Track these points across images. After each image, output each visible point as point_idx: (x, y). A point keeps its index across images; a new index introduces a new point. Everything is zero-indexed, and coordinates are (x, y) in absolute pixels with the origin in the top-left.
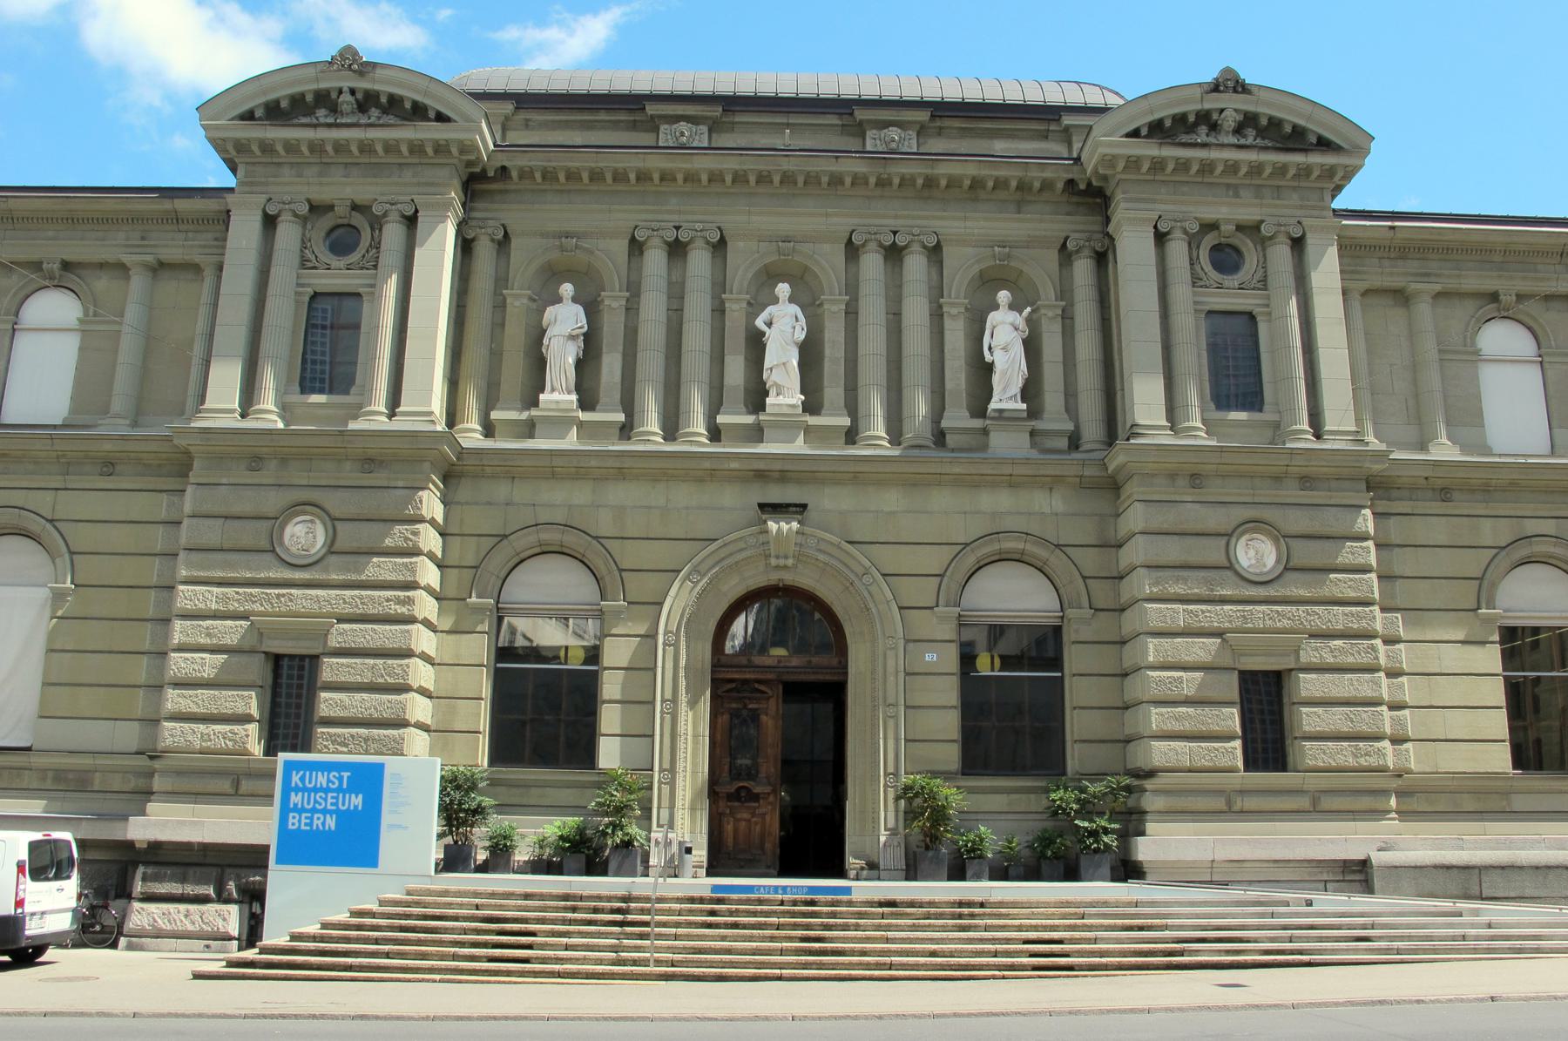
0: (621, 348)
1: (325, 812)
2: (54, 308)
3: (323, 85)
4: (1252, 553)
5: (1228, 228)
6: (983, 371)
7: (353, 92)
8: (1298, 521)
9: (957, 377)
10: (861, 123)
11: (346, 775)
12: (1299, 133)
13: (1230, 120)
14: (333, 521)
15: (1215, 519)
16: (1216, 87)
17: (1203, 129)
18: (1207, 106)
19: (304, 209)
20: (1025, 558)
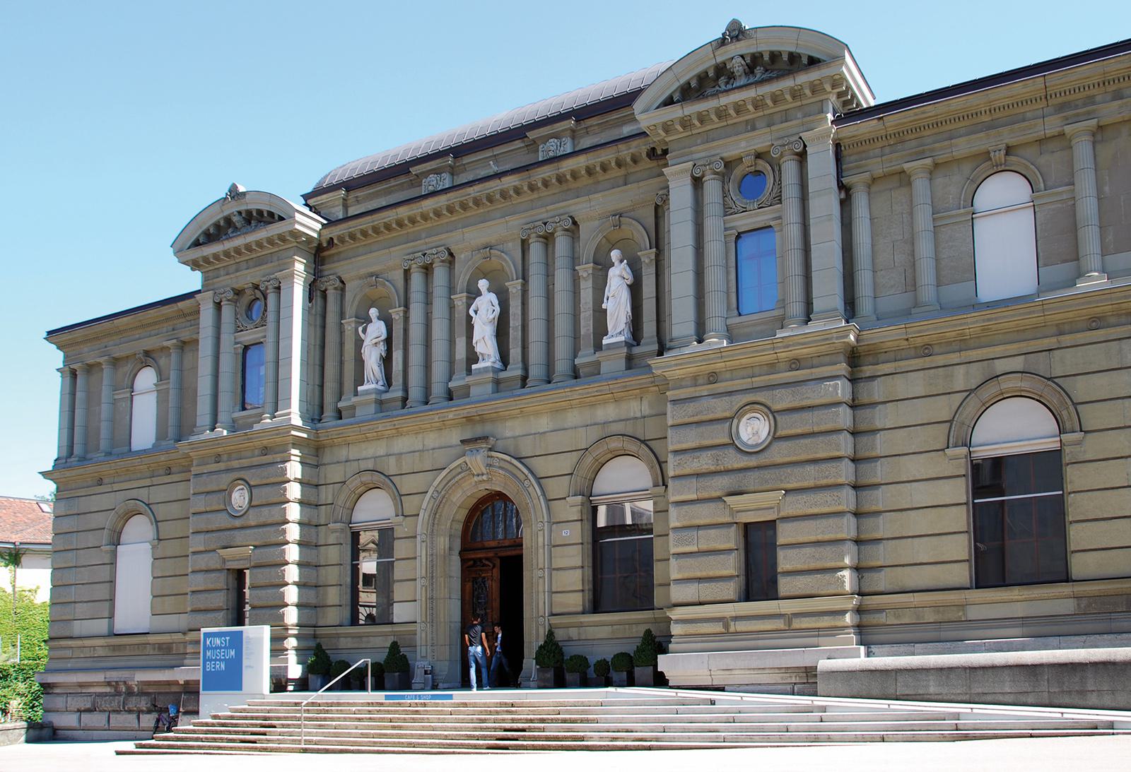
0: (465, 335)
1: (220, 660)
2: (1003, 192)
3: (226, 213)
4: (749, 429)
5: (748, 161)
6: (600, 316)
7: (240, 213)
8: (783, 400)
9: (587, 326)
10: (534, 141)
11: (228, 638)
12: (794, 58)
13: (737, 66)
14: (774, 414)
15: (721, 408)
16: (722, 42)
17: (722, 81)
18: (719, 60)
19: (231, 295)
20: (602, 460)
